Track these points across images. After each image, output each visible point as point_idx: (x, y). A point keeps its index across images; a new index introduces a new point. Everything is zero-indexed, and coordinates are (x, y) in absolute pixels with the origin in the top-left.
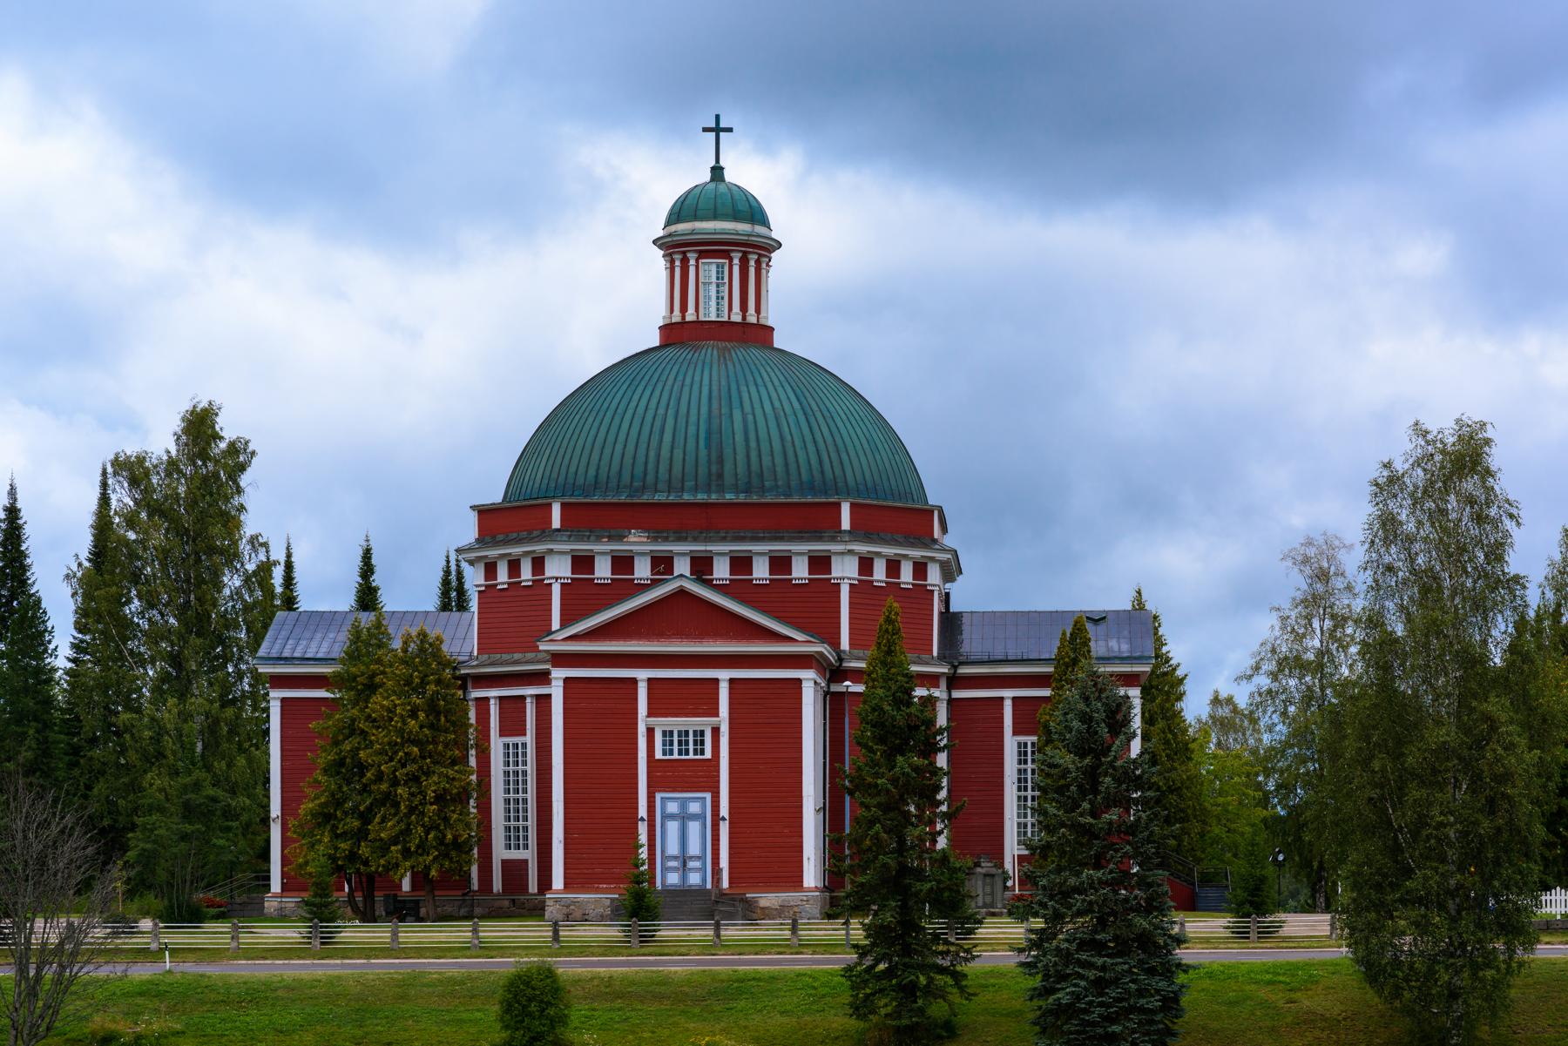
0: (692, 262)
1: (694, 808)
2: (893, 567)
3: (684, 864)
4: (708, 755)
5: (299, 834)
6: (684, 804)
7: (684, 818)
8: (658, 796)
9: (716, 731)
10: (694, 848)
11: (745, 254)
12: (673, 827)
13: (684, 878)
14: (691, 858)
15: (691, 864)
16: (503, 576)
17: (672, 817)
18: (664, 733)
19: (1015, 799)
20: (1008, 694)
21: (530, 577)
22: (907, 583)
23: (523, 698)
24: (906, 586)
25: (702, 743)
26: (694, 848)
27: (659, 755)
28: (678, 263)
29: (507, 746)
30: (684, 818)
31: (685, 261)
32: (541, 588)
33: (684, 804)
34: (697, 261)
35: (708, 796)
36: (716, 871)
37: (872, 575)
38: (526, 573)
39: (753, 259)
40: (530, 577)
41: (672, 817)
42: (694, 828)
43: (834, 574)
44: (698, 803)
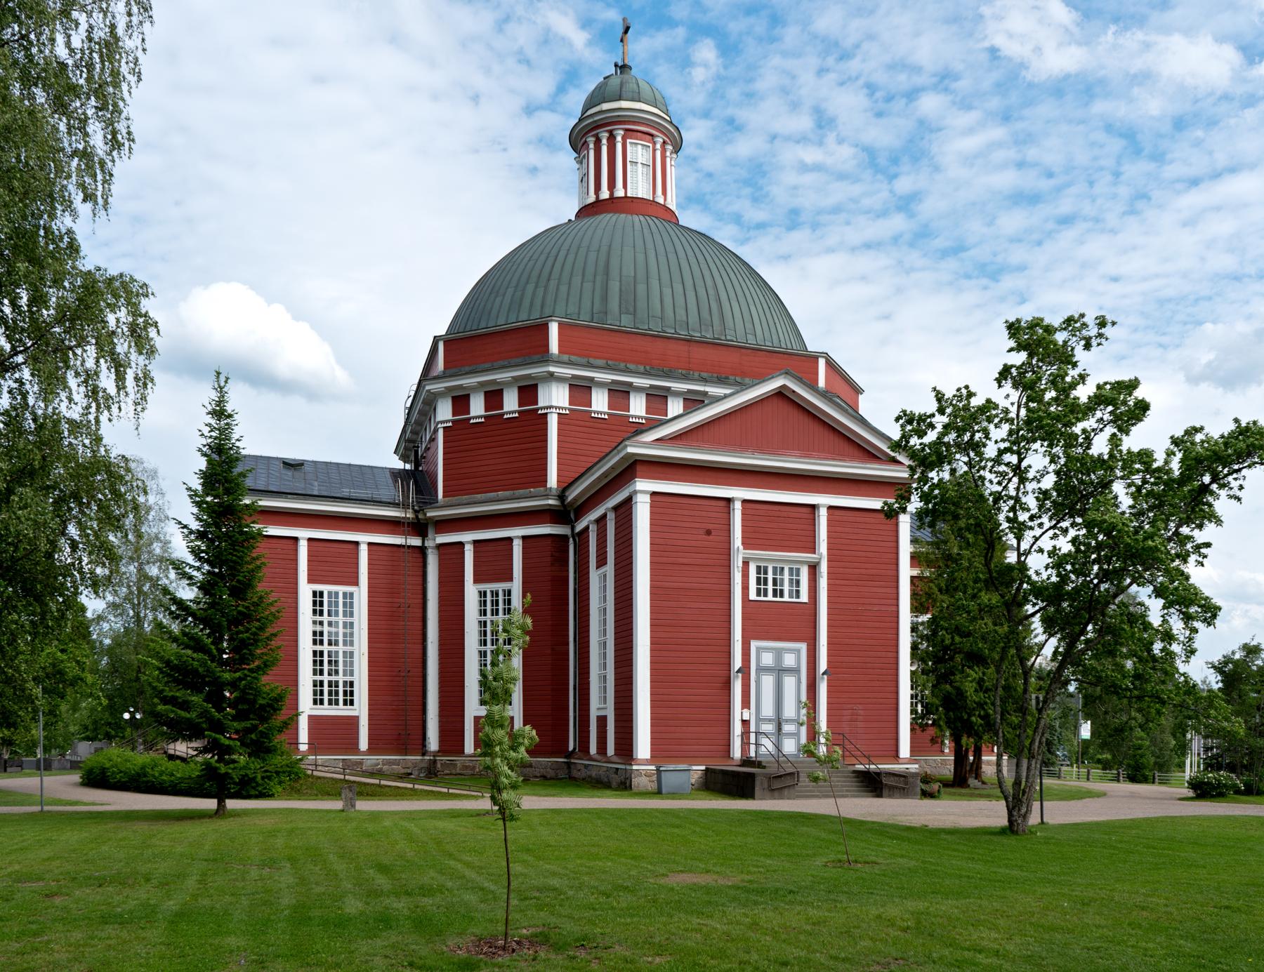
0: (619, 139)
1: (789, 660)
2: (494, 397)
3: (779, 728)
4: (804, 598)
5: (266, 711)
6: (779, 654)
7: (779, 671)
8: (754, 644)
9: (813, 568)
10: (790, 710)
11: (611, 132)
12: (768, 682)
13: (778, 747)
14: (787, 721)
15: (787, 728)
16: (477, 408)
17: (767, 670)
18: (759, 568)
19: (356, 672)
20: (516, 532)
21: (482, 412)
22: (639, 417)
23: (510, 540)
24: (477, 421)
25: (758, 580)
26: (790, 710)
27: (753, 595)
28: (604, 141)
29: (483, 594)
30: (779, 671)
31: (612, 138)
32: (534, 421)
33: (779, 654)
34: (624, 139)
35: (803, 647)
36: (813, 735)
37: (502, 408)
38: (511, 403)
39: (604, 137)
40: (482, 412)
41: (767, 670)
42: (789, 682)
43: (541, 404)
44: (794, 654)
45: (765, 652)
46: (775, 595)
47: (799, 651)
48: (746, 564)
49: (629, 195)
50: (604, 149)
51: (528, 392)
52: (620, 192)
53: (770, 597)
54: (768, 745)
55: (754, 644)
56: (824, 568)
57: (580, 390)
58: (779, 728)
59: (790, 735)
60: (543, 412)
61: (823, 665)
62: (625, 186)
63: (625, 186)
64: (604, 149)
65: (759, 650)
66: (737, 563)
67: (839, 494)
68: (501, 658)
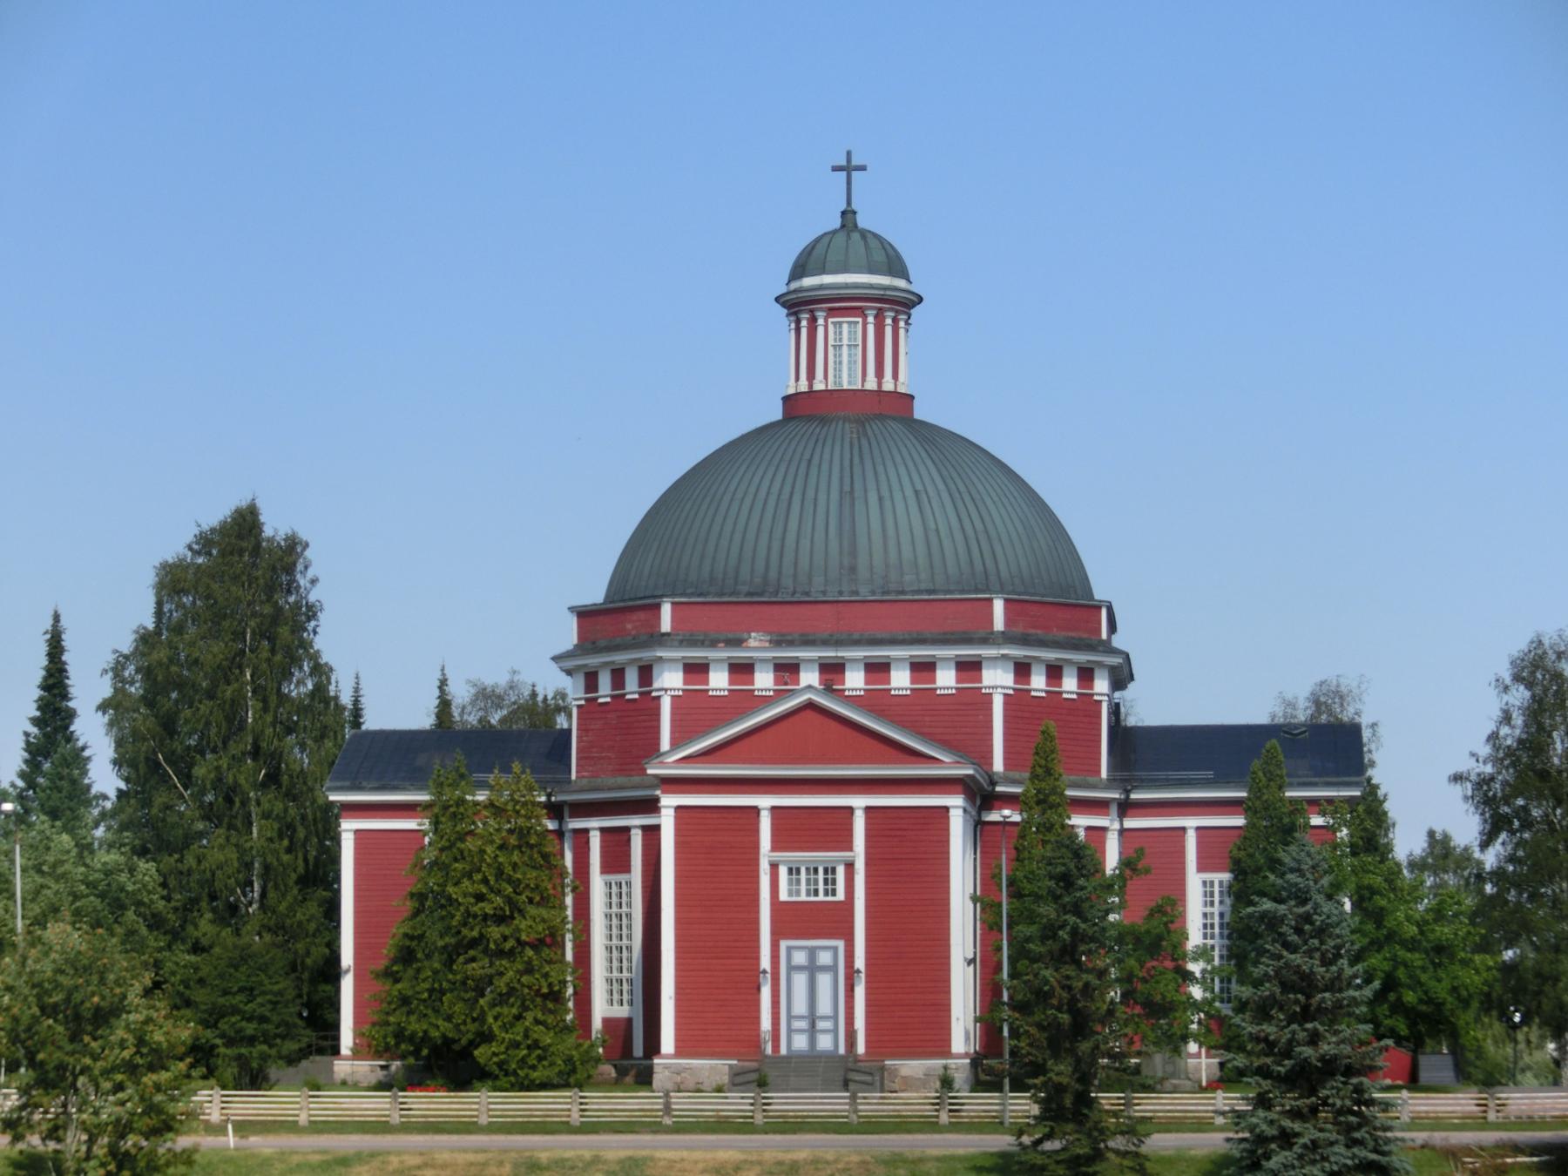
0: (821, 321)
1: (800, 958)
3: (813, 1024)
4: (841, 895)
6: (812, 953)
7: (812, 969)
8: (784, 944)
9: (850, 867)
12: (800, 980)
13: (812, 1041)
17: (800, 968)
21: (609, 692)
26: (824, 1007)
27: (783, 896)
30: (812, 969)
33: (812, 953)
35: (840, 944)
40: (609, 692)
41: (800, 968)
42: (824, 981)
44: (828, 951)
45: (797, 951)
46: (826, 894)
47: (835, 949)
48: (774, 867)
49: (899, 390)
50: (804, 332)
51: (646, 674)
52: (888, 385)
53: (821, 897)
54: (801, 1042)
55: (784, 944)
56: (860, 866)
57: (696, 670)
58: (813, 1024)
59: (825, 1031)
60: (987, 691)
61: (860, 962)
62: (895, 376)
63: (895, 376)
64: (804, 332)
65: (789, 949)
66: (764, 866)
67: (914, 793)
68: (1096, 1134)
